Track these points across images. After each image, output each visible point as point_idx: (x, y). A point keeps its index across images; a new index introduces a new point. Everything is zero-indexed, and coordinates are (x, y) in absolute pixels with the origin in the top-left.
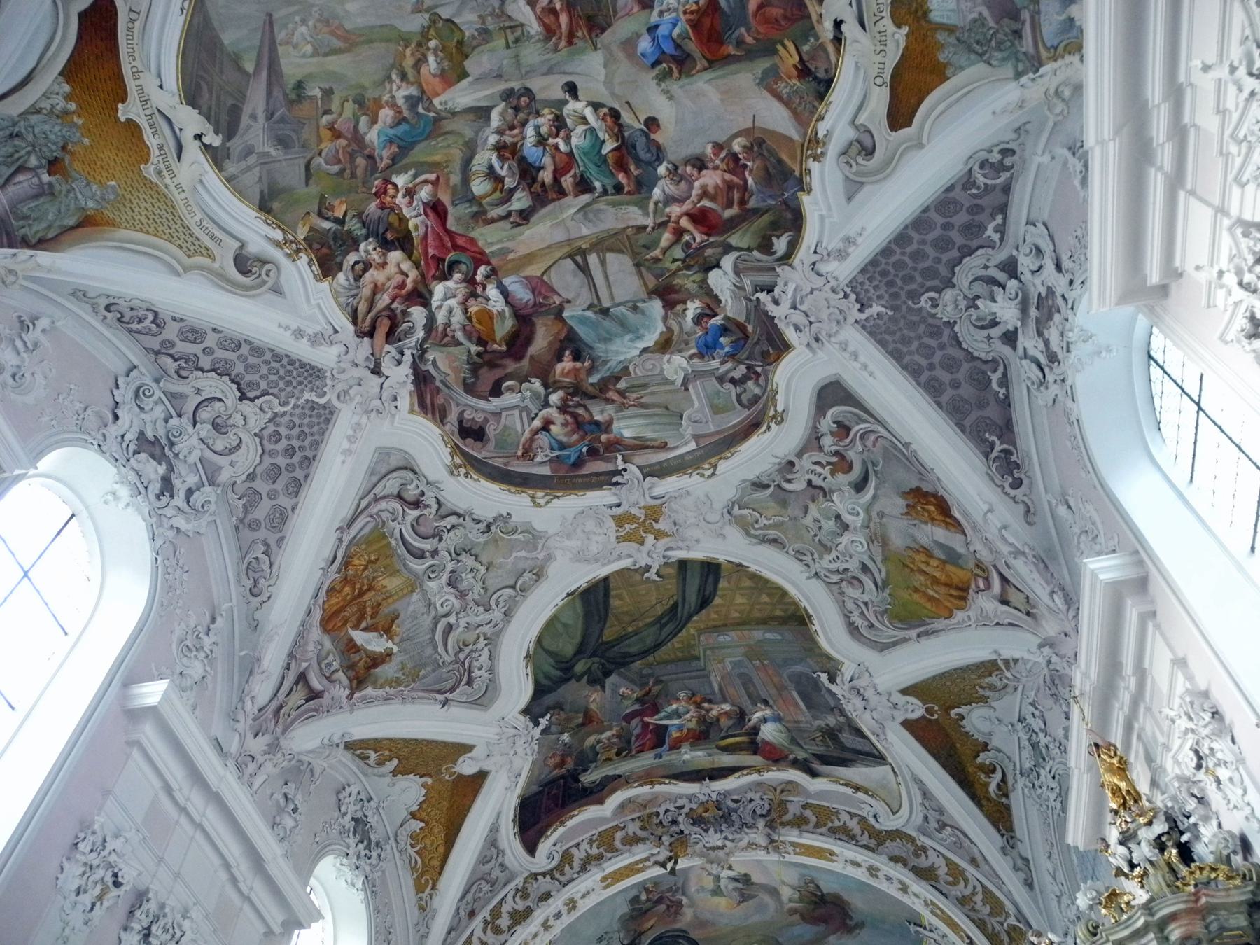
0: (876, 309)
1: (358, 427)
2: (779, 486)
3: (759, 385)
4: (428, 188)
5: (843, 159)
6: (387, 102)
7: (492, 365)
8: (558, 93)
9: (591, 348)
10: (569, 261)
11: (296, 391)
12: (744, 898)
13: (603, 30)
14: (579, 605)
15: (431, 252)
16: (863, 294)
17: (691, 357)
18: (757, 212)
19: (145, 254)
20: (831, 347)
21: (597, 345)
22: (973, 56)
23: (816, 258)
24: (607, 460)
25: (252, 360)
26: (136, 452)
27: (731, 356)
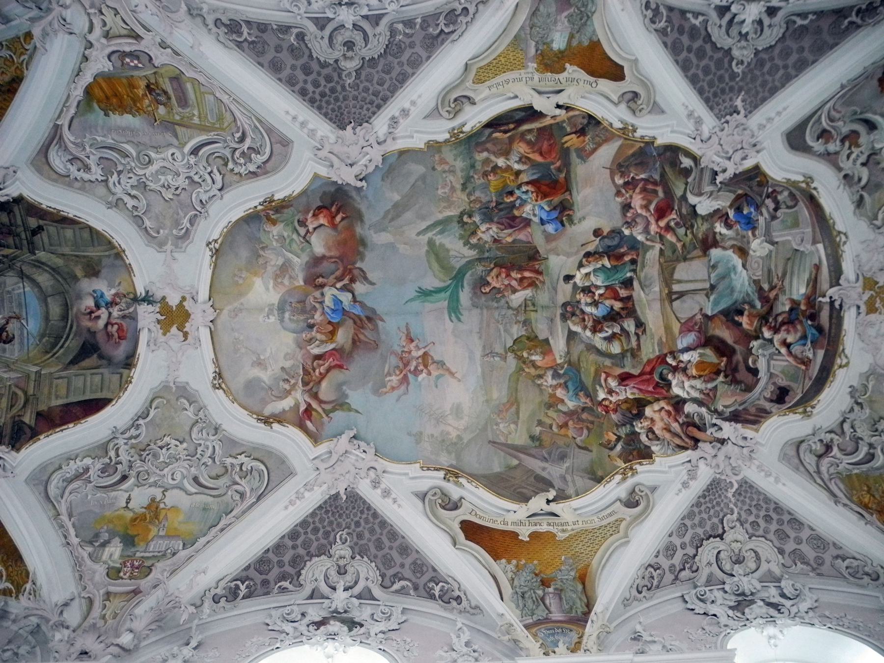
0: (739, 103)
1: (760, 468)
2: (863, 188)
3: (782, 192)
4: (610, 380)
5: (638, 113)
7: (735, 370)
8: (569, 287)
9: (736, 302)
10: (675, 304)
11: (725, 501)
13: (538, 252)
15: (650, 389)
16: (728, 111)
17: (754, 235)
18: (663, 175)
19: (610, 555)
20: (761, 136)
21: (735, 297)
22: (589, 23)
23: (698, 139)
24: (820, 309)
25: (697, 520)
26: (743, 614)
27: (758, 208)
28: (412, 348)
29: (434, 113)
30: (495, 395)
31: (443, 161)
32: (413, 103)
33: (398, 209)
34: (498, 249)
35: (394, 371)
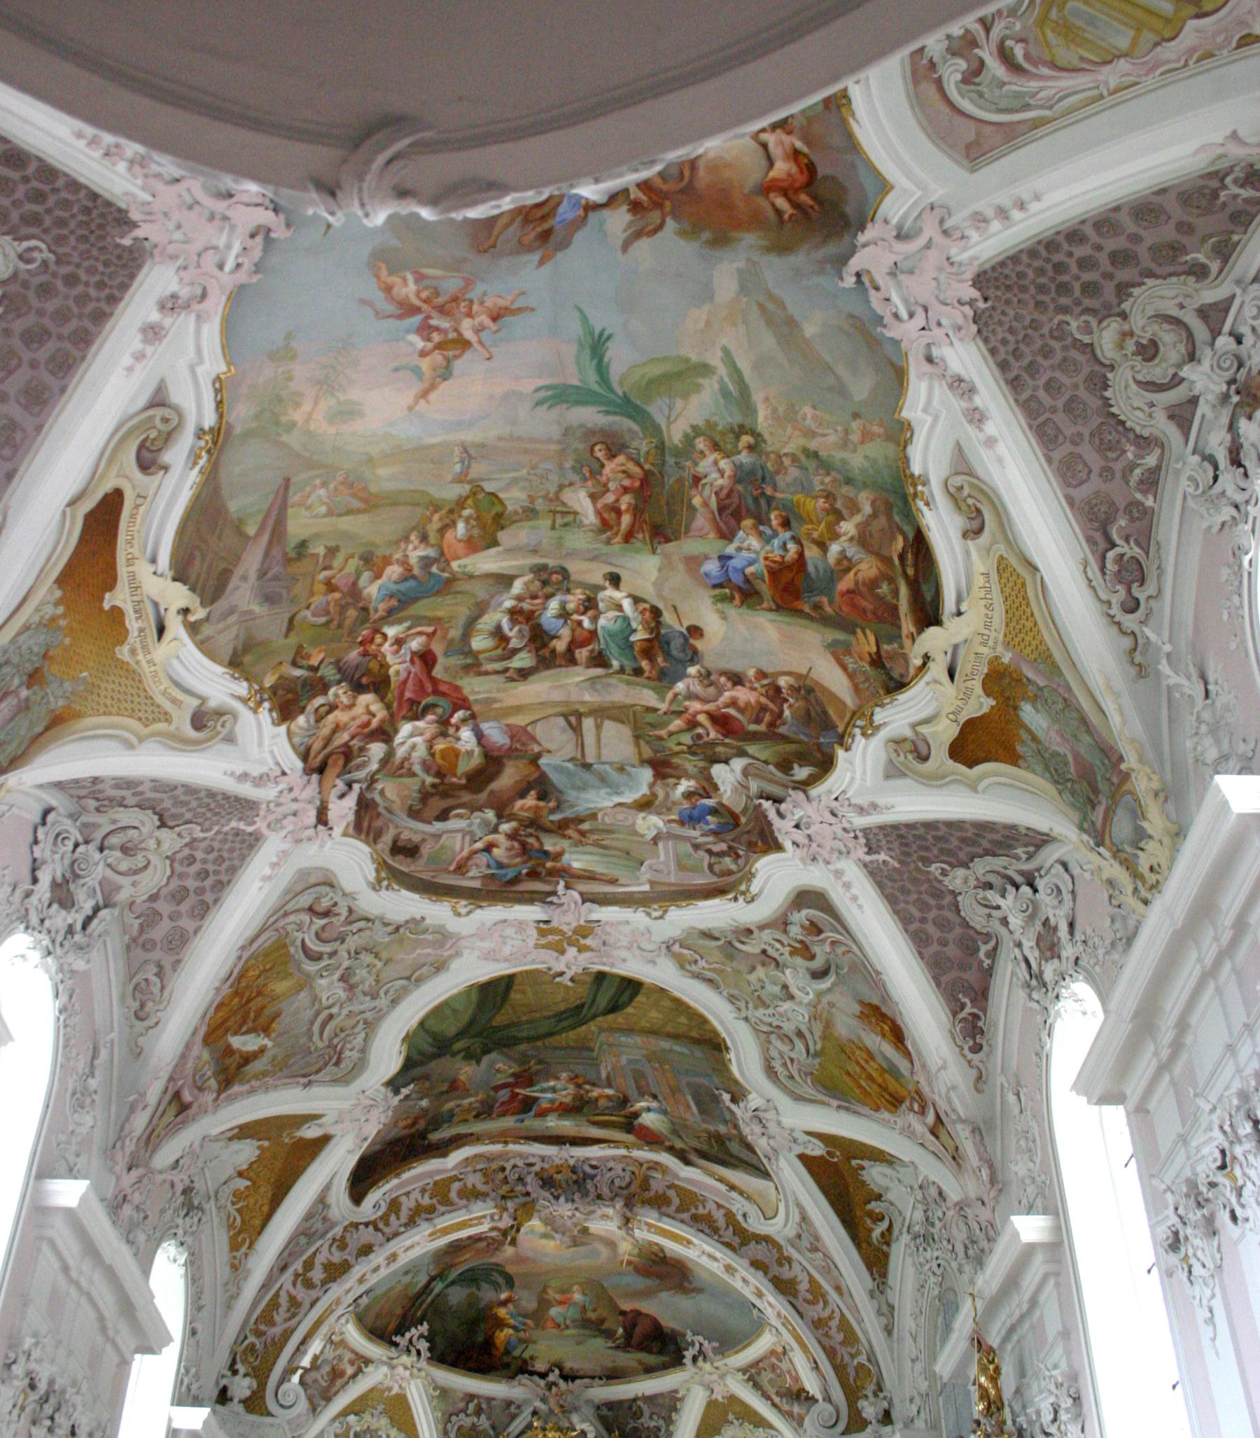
0: (882, 857)
4: (422, 639)
6: (398, 561)
7: (445, 795)
8: (596, 574)
12: (575, 1243)
13: (668, 540)
14: (474, 997)
15: (408, 695)
17: (670, 821)
18: (784, 739)
19: (104, 736)
27: (715, 833)
28: (478, 320)
29: (962, 464)
30: (382, 472)
31: (867, 436)
32: (990, 442)
33: (786, 328)
34: (680, 481)
35: (426, 288)
